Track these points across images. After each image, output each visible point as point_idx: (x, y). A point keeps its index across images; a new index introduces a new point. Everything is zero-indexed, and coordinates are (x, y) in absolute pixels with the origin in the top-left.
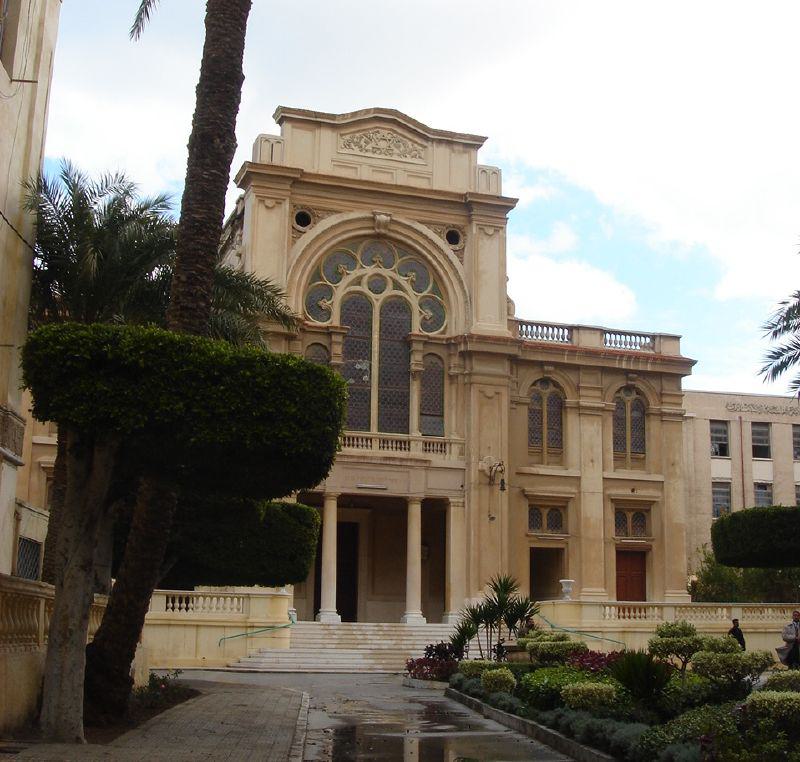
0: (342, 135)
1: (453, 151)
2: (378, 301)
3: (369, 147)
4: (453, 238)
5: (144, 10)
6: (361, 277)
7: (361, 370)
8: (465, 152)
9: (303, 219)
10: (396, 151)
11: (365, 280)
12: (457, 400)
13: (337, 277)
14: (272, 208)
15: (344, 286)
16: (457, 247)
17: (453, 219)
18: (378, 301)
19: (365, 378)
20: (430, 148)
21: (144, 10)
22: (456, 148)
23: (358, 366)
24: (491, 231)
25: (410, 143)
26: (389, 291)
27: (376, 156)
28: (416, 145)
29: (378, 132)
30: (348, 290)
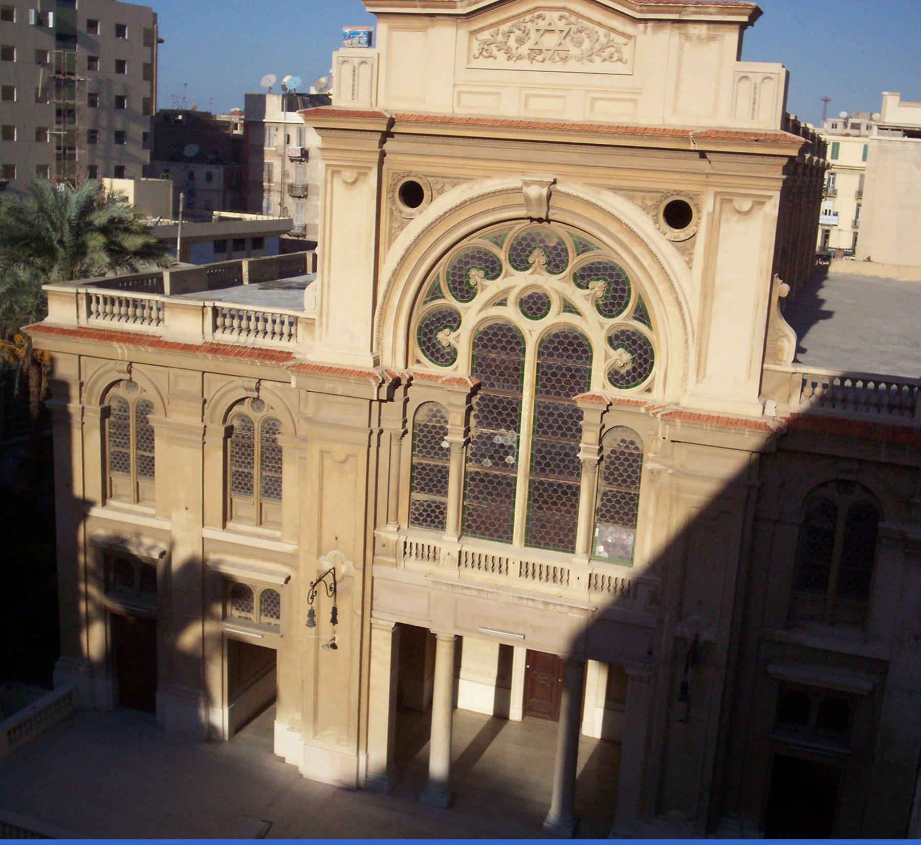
0: (473, 33)
1: (688, 37)
2: (533, 332)
3: (524, 50)
4: (678, 214)
5: (911, 133)
6: (507, 291)
7: (502, 446)
8: (711, 38)
9: (412, 195)
10: (574, 51)
11: (512, 298)
12: (656, 509)
13: (465, 293)
14: (749, 212)
15: (479, 306)
16: (681, 234)
17: (677, 184)
18: (533, 332)
19: (510, 459)
20: (641, 39)
21: (911, 133)
22: (694, 30)
23: (498, 440)
24: (746, 205)
25: (602, 32)
26: (554, 318)
27: (536, 66)
28: (613, 35)
29: (539, 17)
30: (483, 315)
